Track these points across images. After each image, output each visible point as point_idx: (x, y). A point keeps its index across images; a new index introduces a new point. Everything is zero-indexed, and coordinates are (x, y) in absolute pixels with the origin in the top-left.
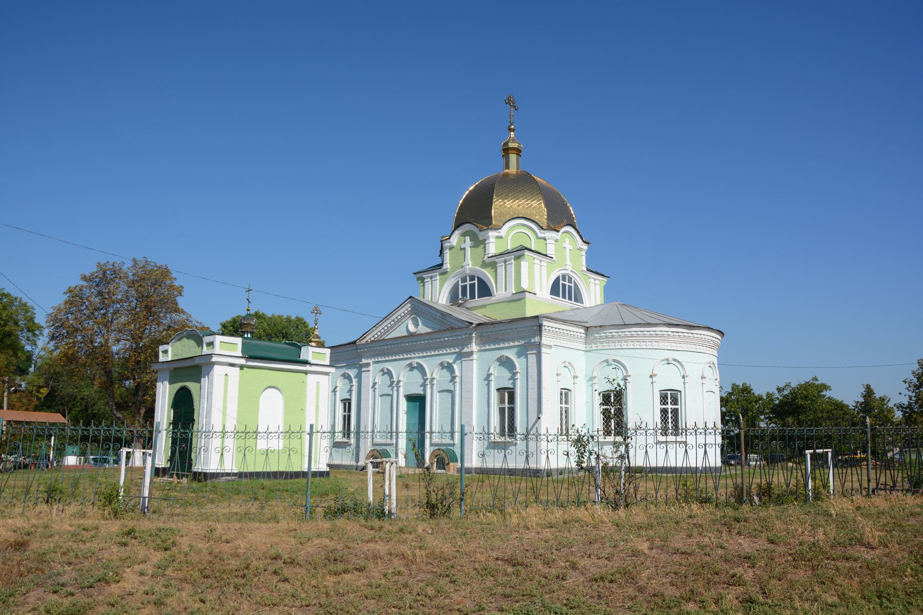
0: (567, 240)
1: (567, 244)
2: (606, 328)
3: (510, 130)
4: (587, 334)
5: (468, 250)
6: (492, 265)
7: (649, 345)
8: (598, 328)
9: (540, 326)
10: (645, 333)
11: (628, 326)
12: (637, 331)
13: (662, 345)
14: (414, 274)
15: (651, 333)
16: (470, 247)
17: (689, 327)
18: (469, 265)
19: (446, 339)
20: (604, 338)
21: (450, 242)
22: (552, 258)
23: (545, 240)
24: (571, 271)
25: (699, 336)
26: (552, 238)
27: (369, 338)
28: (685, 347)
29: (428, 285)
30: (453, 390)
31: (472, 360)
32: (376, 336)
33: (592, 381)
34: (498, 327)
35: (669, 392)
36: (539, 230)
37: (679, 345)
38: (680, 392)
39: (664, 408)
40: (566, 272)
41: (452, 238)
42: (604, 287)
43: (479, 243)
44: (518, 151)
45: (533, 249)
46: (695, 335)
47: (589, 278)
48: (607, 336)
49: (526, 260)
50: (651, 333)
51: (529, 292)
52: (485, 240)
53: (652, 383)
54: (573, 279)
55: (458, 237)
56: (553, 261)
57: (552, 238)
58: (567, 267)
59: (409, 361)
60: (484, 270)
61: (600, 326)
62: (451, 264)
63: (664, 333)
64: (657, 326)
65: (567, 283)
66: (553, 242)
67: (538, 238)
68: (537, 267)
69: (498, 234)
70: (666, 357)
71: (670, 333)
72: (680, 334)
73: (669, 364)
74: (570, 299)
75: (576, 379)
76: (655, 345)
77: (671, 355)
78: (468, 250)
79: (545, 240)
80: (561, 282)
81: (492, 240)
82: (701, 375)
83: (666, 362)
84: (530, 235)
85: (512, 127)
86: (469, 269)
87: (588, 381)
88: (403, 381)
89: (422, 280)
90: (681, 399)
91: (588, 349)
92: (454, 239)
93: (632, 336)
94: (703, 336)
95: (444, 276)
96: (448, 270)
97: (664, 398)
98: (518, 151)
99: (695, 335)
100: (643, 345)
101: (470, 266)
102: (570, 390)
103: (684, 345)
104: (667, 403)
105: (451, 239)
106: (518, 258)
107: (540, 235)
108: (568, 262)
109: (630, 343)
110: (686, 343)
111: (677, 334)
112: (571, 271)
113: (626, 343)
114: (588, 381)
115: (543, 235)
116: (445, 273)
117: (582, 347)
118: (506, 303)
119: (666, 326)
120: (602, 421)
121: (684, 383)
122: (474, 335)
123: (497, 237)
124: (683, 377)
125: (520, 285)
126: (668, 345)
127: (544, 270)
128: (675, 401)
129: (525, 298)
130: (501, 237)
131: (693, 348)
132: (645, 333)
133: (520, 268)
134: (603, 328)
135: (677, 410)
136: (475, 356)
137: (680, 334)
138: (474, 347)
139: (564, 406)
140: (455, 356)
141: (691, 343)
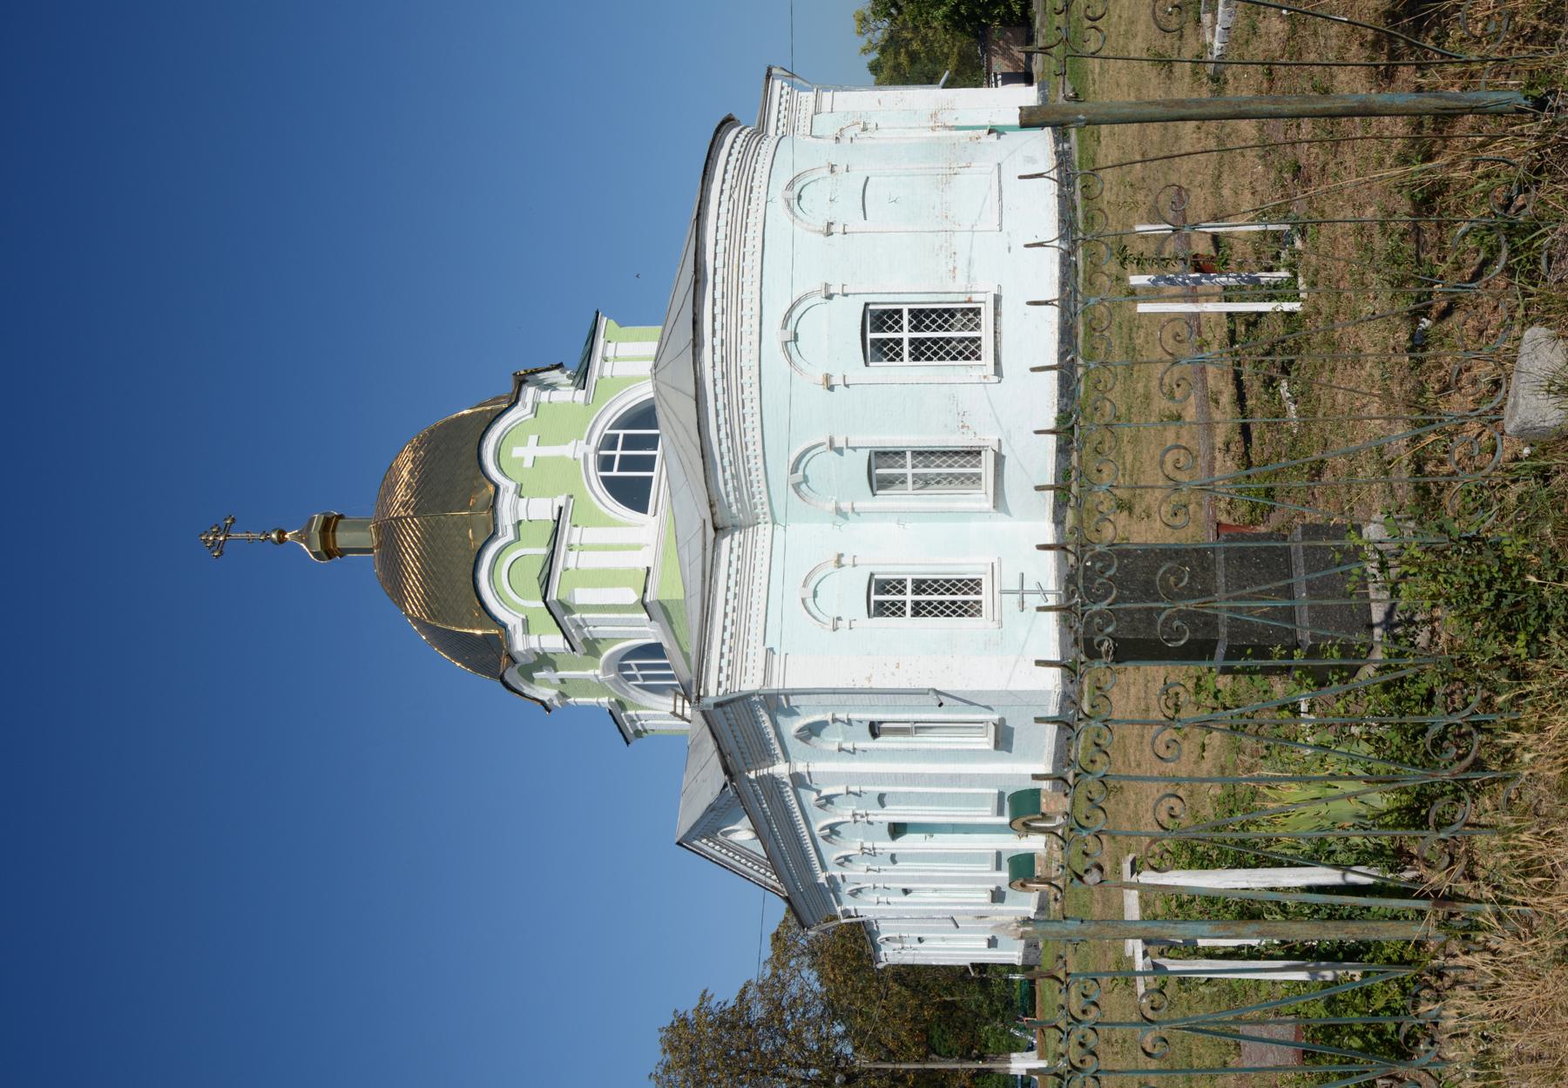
0: (517, 452)
1: (525, 452)
2: (713, 492)
3: (281, 540)
4: (735, 527)
5: (561, 674)
6: (592, 647)
7: (751, 392)
8: (717, 509)
9: (718, 705)
10: (720, 406)
11: (706, 448)
12: (717, 411)
13: (748, 359)
14: (628, 743)
15: (719, 390)
16: (556, 671)
17: (700, 285)
18: (596, 676)
19: (765, 806)
20: (741, 494)
21: (551, 700)
22: (561, 509)
23: (520, 522)
24: (588, 442)
25: (720, 249)
26: (515, 508)
27: (772, 880)
28: (750, 306)
29: (650, 724)
30: (868, 450)
31: (809, 773)
32: (768, 874)
33: (842, 448)
34: (730, 745)
35: (870, 336)
36: (498, 538)
37: (746, 310)
38: (867, 304)
39: (913, 609)
40: (592, 458)
41: (540, 698)
42: (621, 324)
43: (544, 660)
44: (329, 526)
45: (544, 551)
46: (719, 263)
47: (601, 377)
48: (735, 489)
49: (572, 594)
50: (719, 390)
51: (645, 591)
52: (537, 654)
53: (847, 386)
54: (607, 431)
55: (538, 688)
56: (567, 503)
57: (515, 508)
58: (580, 456)
59: (821, 842)
60: (606, 654)
61: (711, 506)
62: (599, 696)
63: (718, 358)
64: (702, 376)
65: (618, 453)
66: (523, 502)
67: (518, 538)
68: (590, 561)
69: (520, 629)
70: (779, 347)
71: (717, 341)
72: (718, 310)
73: (796, 335)
74: (652, 442)
75: (844, 561)
76: (750, 376)
77: (774, 335)
78: (561, 674)
79: (520, 522)
80: (615, 473)
81: (534, 642)
82: (822, 236)
83: (791, 346)
84: (506, 585)
85: (274, 536)
86: (604, 672)
87: (847, 519)
88: (862, 843)
89: (638, 733)
90: (884, 302)
91: (768, 518)
92: (544, 695)
93: (731, 435)
94: (721, 236)
95: (627, 705)
96: (613, 700)
97: (884, 351)
98: (329, 526)
99: (719, 263)
100: (751, 408)
101: (598, 672)
102: (872, 575)
103: (746, 295)
104: (901, 328)
105: (545, 699)
106: (567, 608)
107: (510, 536)
108: (567, 450)
109: (749, 438)
110: (740, 286)
111: (719, 318)
112: (588, 442)
113: (750, 445)
114: (847, 519)
115: (510, 530)
116: (621, 705)
117: (764, 531)
118: (675, 626)
119: (700, 354)
120: (935, 362)
121: (846, 295)
122: (752, 775)
123: (527, 631)
124: (829, 297)
125: (629, 606)
126: (750, 338)
127: (591, 535)
128: (898, 586)
129: (659, 602)
130: (526, 623)
131: (752, 262)
132: (720, 406)
133: (592, 605)
134: (715, 498)
135: (915, 314)
136: (800, 767)
137: (718, 310)
138: (780, 769)
139: (909, 598)
140: (802, 791)
141: (741, 272)
